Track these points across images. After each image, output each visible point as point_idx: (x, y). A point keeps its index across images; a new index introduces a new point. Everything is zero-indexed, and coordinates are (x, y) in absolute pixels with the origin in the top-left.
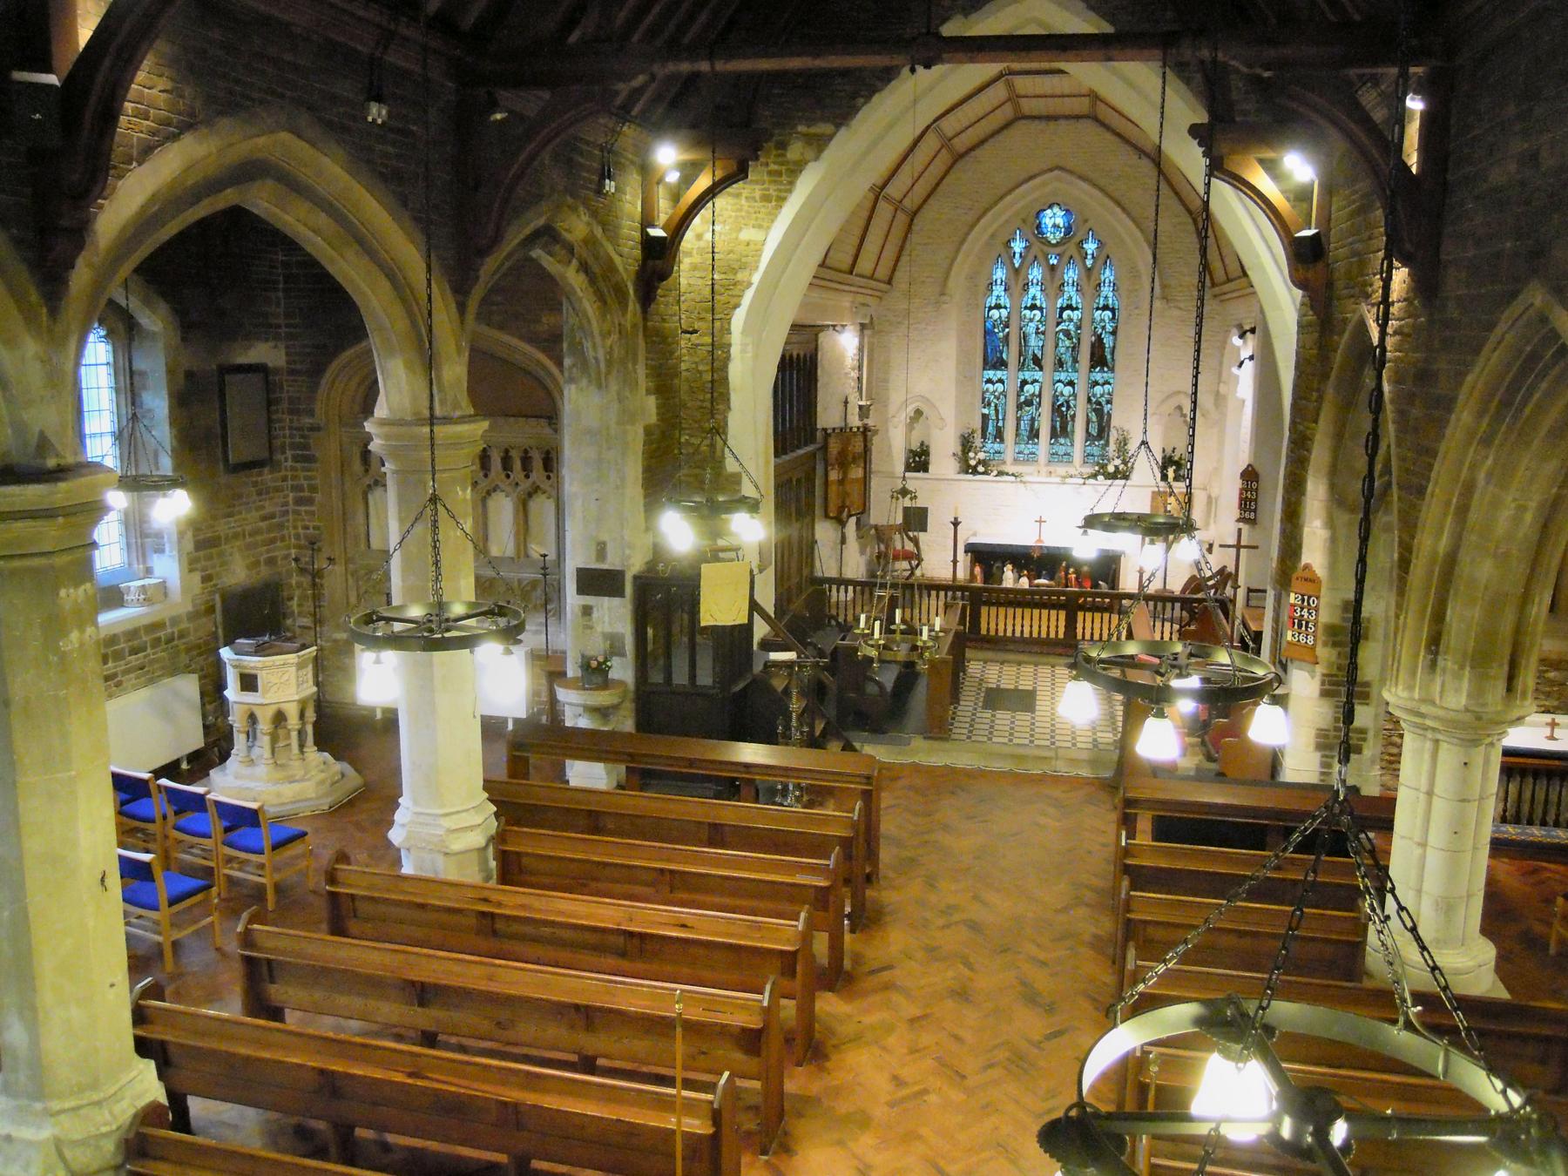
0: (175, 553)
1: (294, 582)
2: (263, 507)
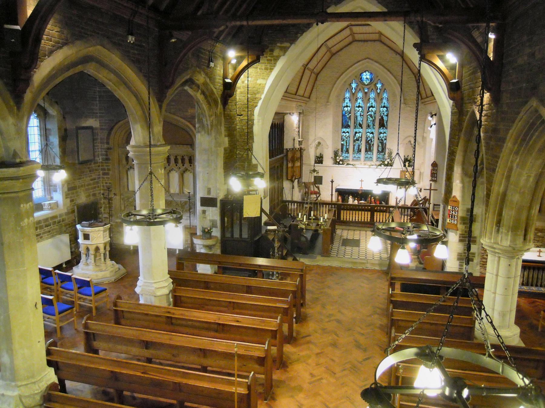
0: (61, 192)
1: (102, 202)
2: (91, 176)
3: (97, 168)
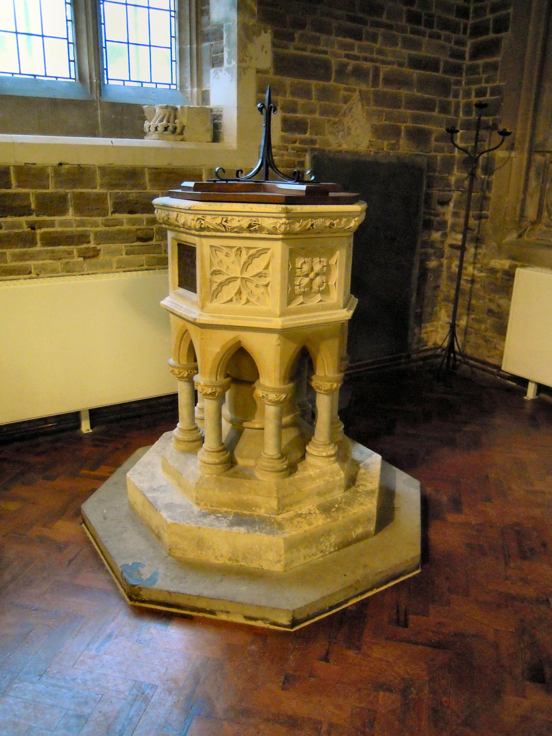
0: (234, 63)
1: (453, 179)
2: (417, 45)
3: (452, 17)
